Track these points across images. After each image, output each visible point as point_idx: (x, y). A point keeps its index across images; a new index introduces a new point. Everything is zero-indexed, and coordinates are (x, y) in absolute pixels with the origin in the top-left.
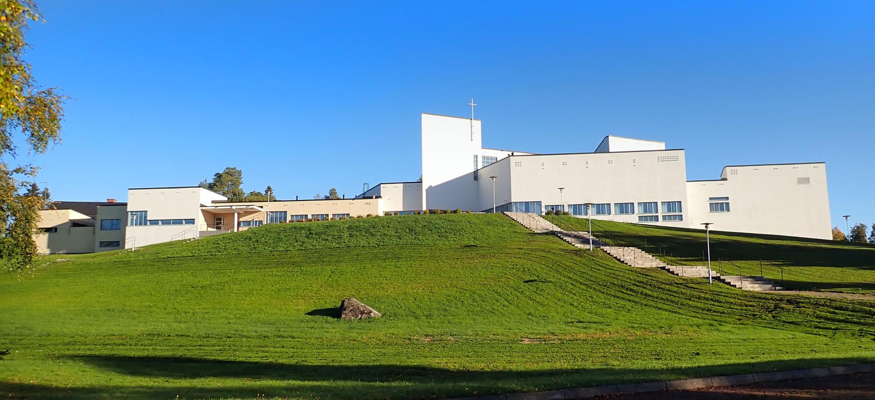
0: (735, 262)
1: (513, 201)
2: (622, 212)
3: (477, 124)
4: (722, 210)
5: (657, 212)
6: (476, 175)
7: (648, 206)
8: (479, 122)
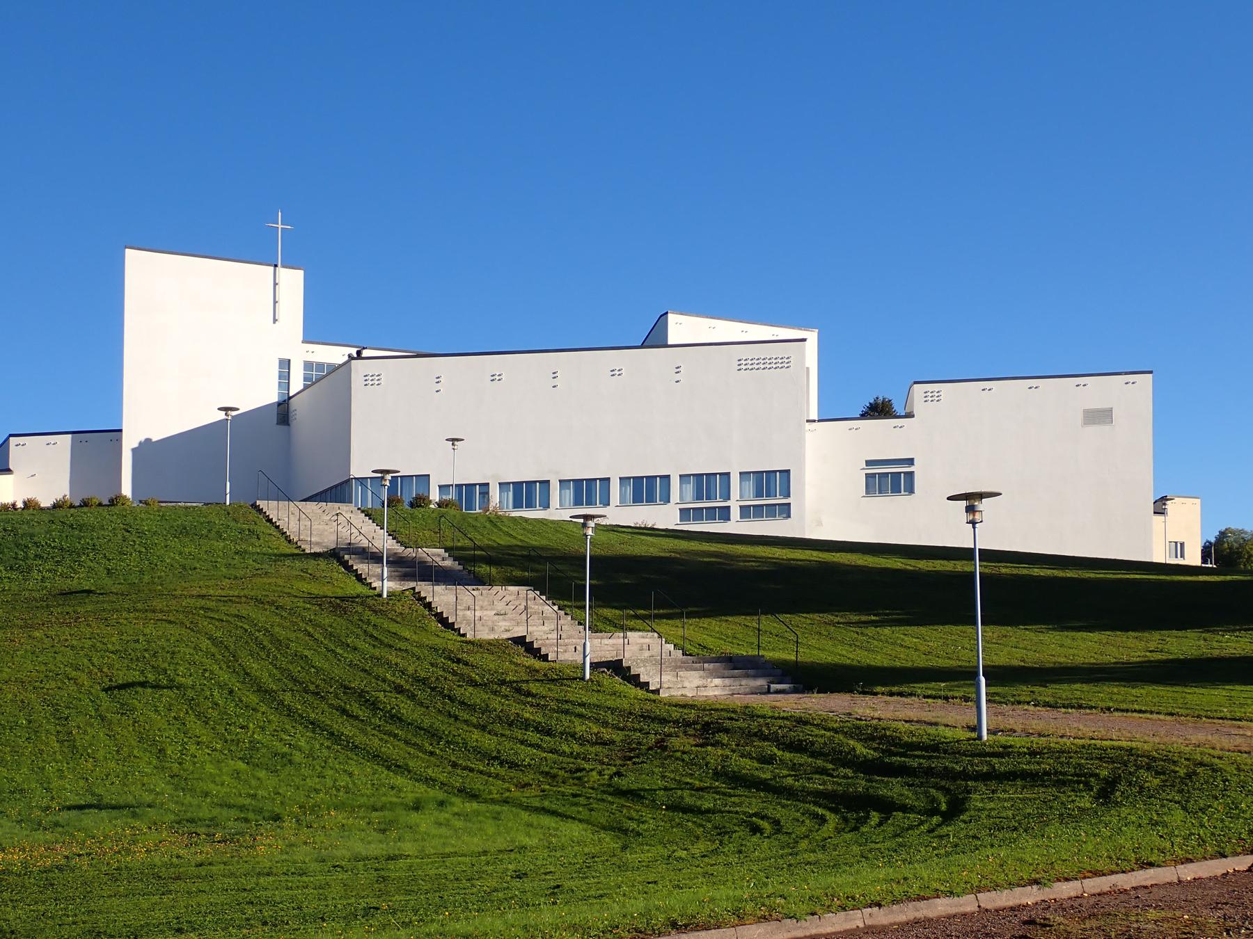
0: (781, 617)
1: (356, 472)
2: (637, 499)
3: (293, 281)
4: (896, 490)
5: (727, 497)
6: (283, 411)
7: (707, 484)
8: (299, 275)
